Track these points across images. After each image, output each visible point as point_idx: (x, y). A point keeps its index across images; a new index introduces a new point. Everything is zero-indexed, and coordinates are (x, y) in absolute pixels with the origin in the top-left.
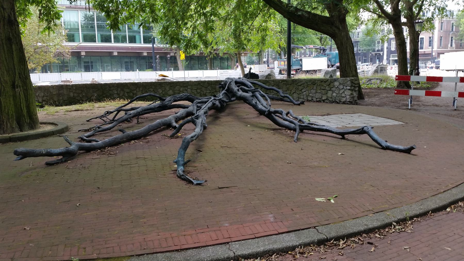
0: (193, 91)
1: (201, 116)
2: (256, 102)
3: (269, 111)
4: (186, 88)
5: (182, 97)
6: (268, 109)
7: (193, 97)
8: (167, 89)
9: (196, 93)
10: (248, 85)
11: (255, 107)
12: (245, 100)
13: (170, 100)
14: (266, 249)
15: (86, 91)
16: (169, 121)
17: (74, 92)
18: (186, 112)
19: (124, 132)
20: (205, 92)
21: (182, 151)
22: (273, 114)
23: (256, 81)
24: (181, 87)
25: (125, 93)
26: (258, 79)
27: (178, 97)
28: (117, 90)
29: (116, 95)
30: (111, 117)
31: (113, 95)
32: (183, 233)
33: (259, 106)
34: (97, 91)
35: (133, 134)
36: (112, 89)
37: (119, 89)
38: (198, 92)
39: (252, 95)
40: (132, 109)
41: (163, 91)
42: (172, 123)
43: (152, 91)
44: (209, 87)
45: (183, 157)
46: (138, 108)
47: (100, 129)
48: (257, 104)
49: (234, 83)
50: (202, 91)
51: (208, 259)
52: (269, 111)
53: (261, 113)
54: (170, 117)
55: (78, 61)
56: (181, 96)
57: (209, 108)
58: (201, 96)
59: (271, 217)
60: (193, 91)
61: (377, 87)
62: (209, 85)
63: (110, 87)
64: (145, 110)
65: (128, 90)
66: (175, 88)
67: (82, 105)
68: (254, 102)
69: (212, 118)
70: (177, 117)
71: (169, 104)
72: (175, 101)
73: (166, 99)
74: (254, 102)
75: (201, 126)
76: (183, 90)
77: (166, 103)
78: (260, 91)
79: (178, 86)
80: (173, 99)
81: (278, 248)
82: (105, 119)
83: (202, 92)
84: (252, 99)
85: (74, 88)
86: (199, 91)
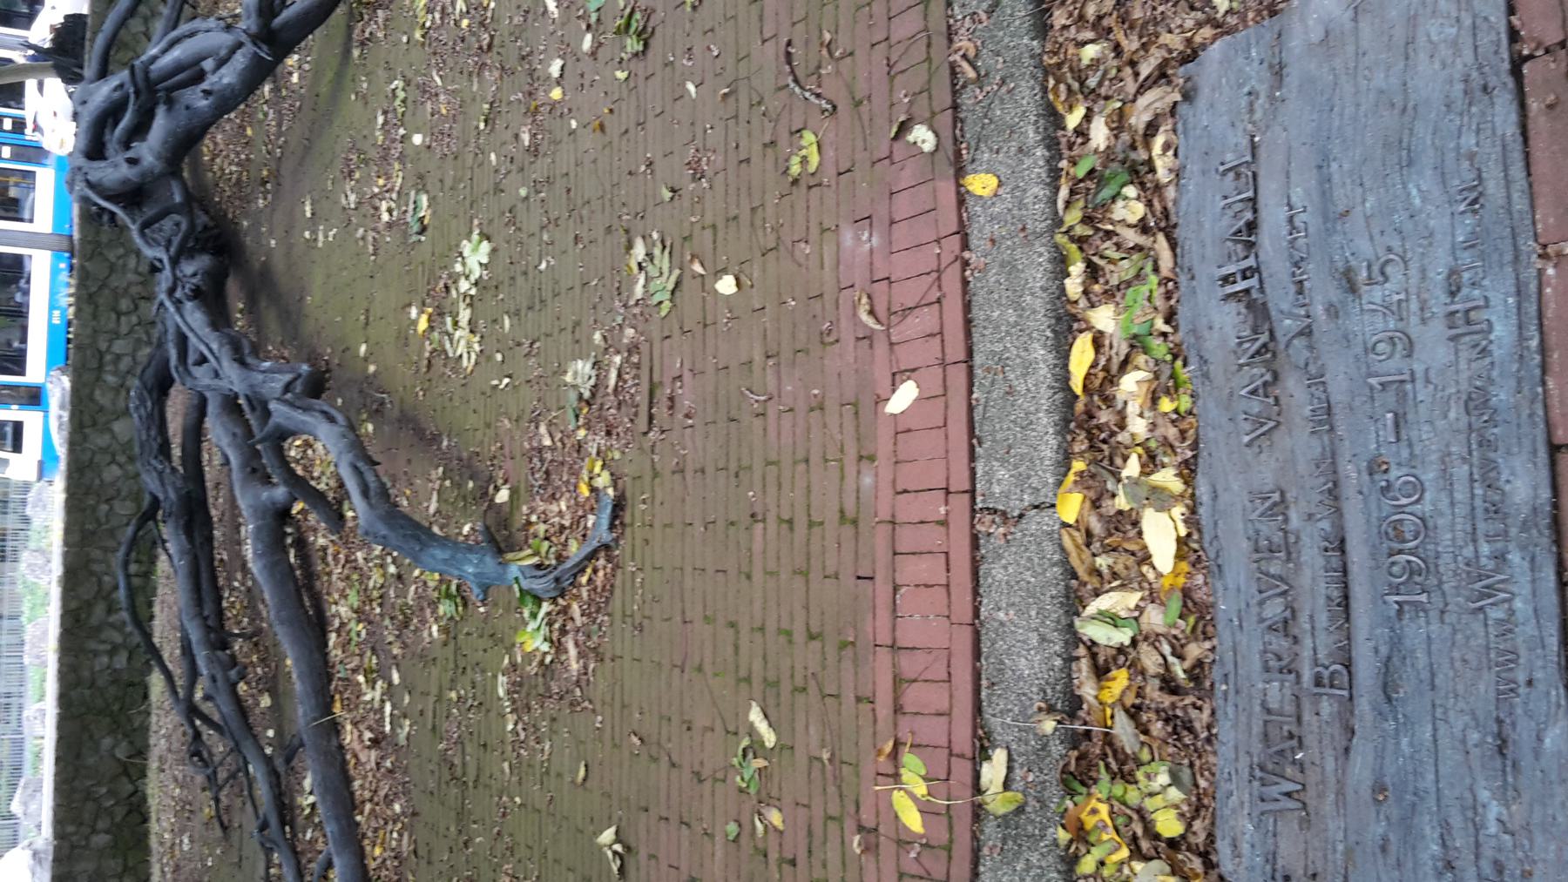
0: (124, 329)
1: (252, 386)
2: (204, 91)
3: (256, 39)
4: (108, 358)
5: (150, 416)
6: (244, 38)
7: (153, 363)
8: (102, 440)
9: (134, 319)
10: (108, 97)
11: (227, 102)
12: (185, 144)
13: (160, 474)
14: (1048, 333)
15: (89, 783)
16: (263, 518)
17: (89, 830)
18: (225, 419)
19: (296, 742)
20: (131, 277)
21: (433, 557)
22: (278, 21)
23: (93, 40)
24: (98, 379)
25: (111, 619)
26: (89, 21)
27: (149, 436)
28: (96, 654)
29: (116, 659)
30: (218, 745)
31: (115, 670)
32: (884, 709)
33: (226, 81)
34: (91, 737)
35: (313, 701)
36: (86, 674)
37: (92, 645)
38: (132, 307)
39: (165, 103)
40: (187, 650)
41: (113, 461)
42: (274, 504)
43: (111, 509)
44: (112, 256)
45: (459, 556)
46: (183, 629)
47: (274, 821)
48: (216, 88)
49: (96, 164)
50: (126, 290)
51: (1057, 648)
52: (256, 39)
53: (260, 72)
54: (242, 503)
55: (70, 155)
56: (140, 417)
57: (215, 326)
58: (149, 298)
59: (858, 238)
60: (124, 329)
61: (285, 348)
62: (101, 254)
63: (78, 683)
64: (198, 601)
65: (99, 609)
66: (101, 409)
67: (153, 803)
68: (205, 102)
69: (263, 304)
70: (244, 465)
71: (179, 483)
72: (164, 449)
73: (151, 493)
74: (205, 102)
75: (306, 409)
76: (115, 373)
77: (172, 495)
78: (144, 58)
79: (92, 393)
80: (154, 462)
81: (1049, 266)
82: (222, 775)
83: (134, 290)
84: (188, 108)
85: (70, 829)
86: (124, 304)
